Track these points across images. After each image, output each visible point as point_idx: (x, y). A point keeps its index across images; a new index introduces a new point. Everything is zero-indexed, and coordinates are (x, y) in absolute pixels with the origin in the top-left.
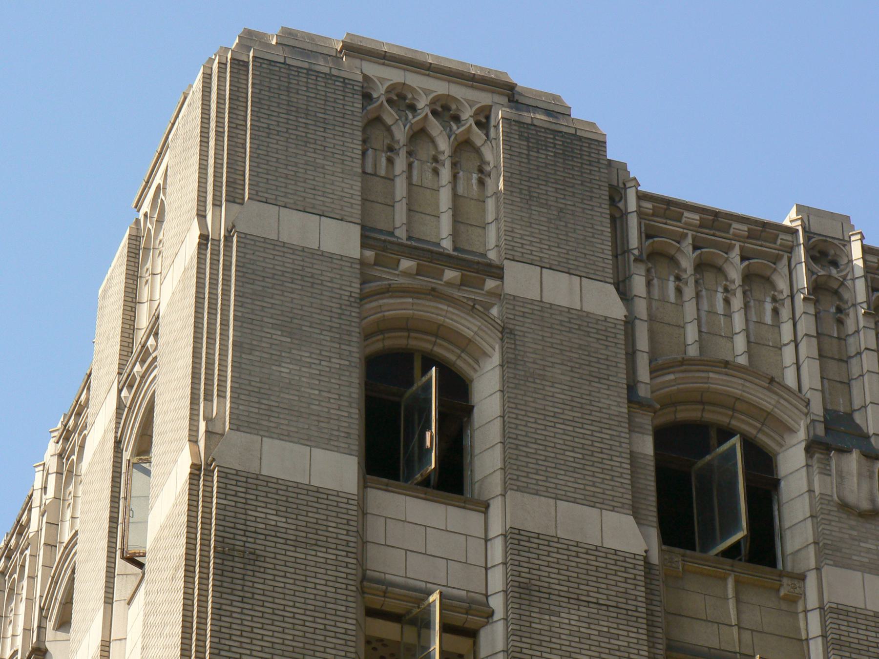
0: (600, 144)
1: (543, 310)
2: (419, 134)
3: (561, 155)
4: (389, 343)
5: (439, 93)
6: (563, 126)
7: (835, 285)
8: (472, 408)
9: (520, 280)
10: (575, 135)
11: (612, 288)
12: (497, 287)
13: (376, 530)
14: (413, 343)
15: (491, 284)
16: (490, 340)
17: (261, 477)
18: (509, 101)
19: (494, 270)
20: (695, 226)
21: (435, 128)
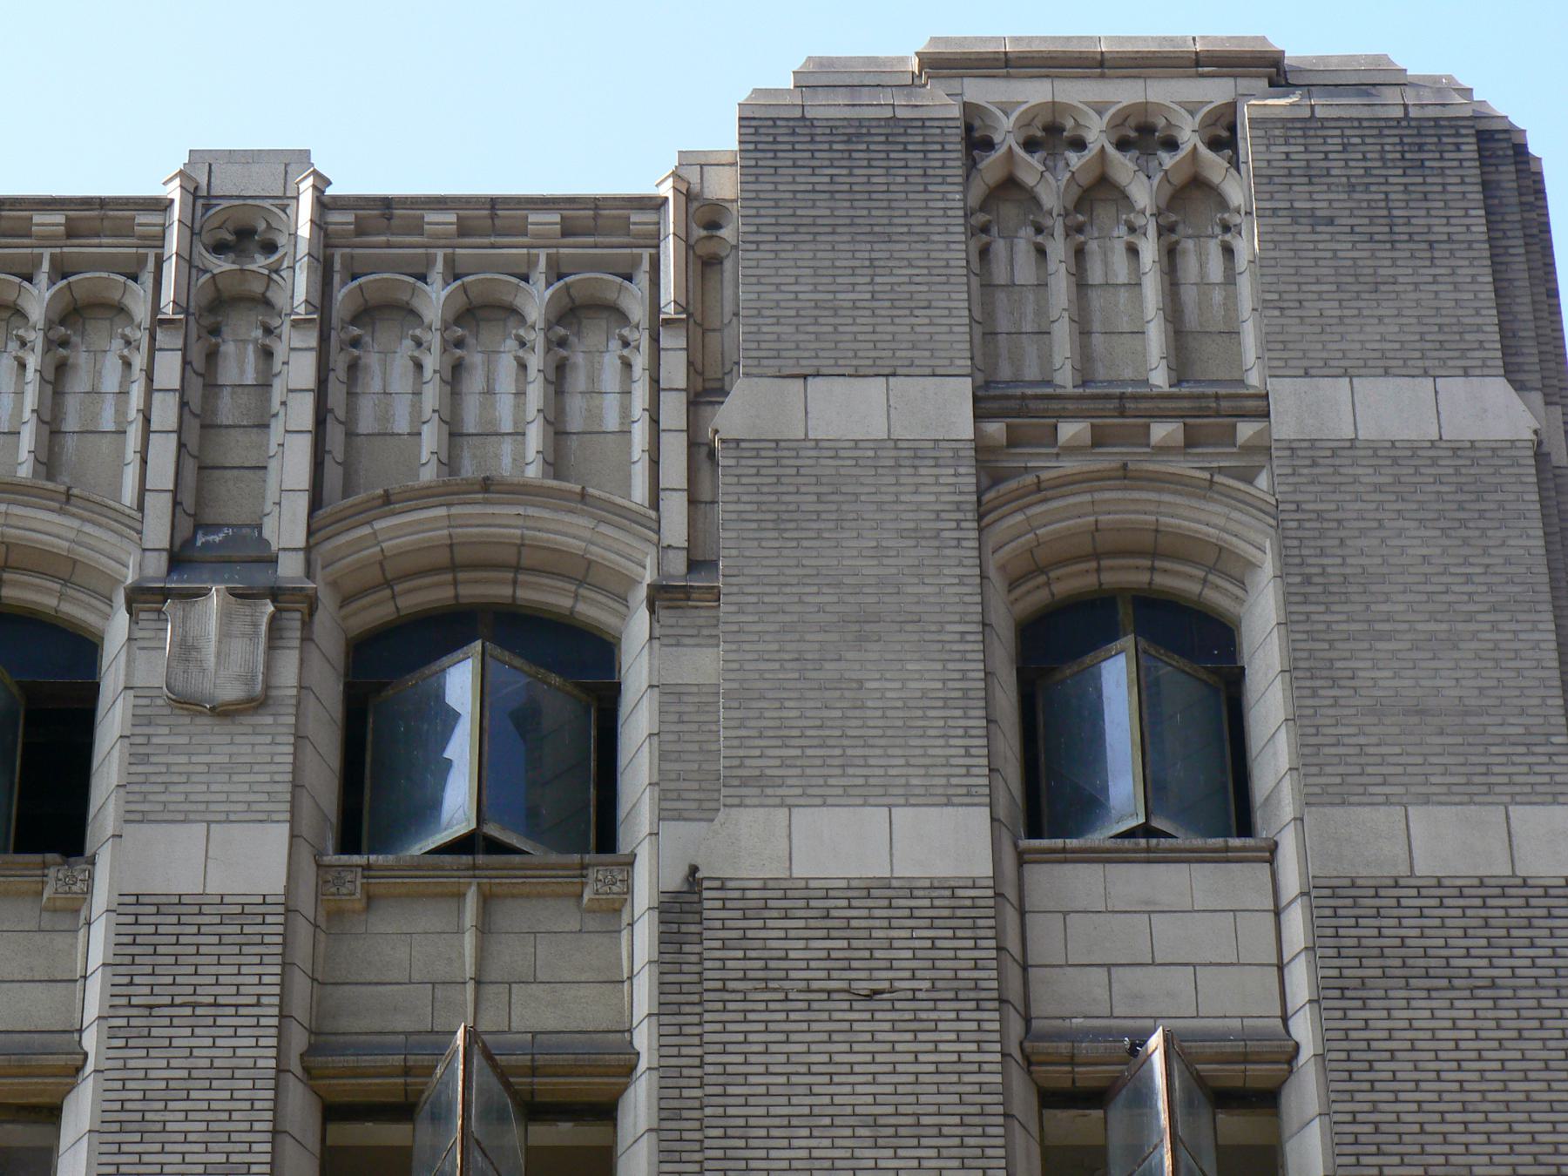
2: (1099, 191)
5: (1033, 102)
6: (1391, 104)
7: (257, 287)
8: (1243, 669)
9: (1308, 408)
10: (894, 118)
12: (1259, 434)
13: (1046, 940)
14: (1110, 579)
15: (1246, 430)
16: (1252, 536)
17: (895, 883)
18: (1271, 85)
19: (1144, 405)
20: (446, 236)
21: (1123, 167)
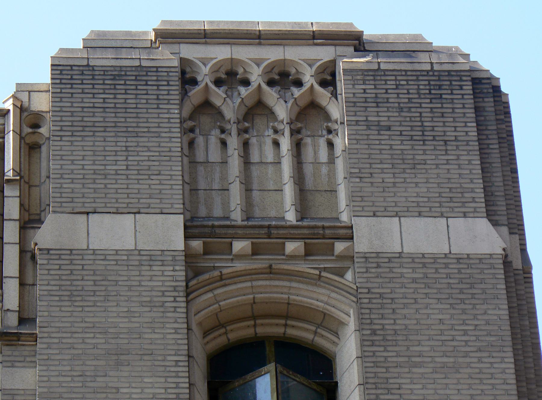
2: (257, 109)
4: (234, 336)
5: (220, 58)
6: (424, 62)
9: (374, 234)
11: (485, 220)
12: (347, 249)
14: (261, 331)
15: (340, 247)
16: (343, 307)
18: (356, 50)
21: (271, 96)
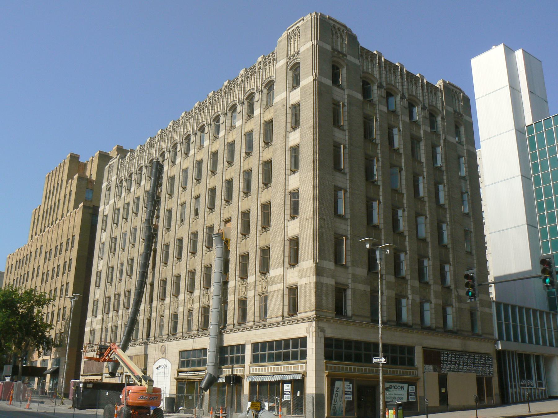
0: (357, 38)
1: (351, 62)
3: (353, 39)
9: (349, 57)
